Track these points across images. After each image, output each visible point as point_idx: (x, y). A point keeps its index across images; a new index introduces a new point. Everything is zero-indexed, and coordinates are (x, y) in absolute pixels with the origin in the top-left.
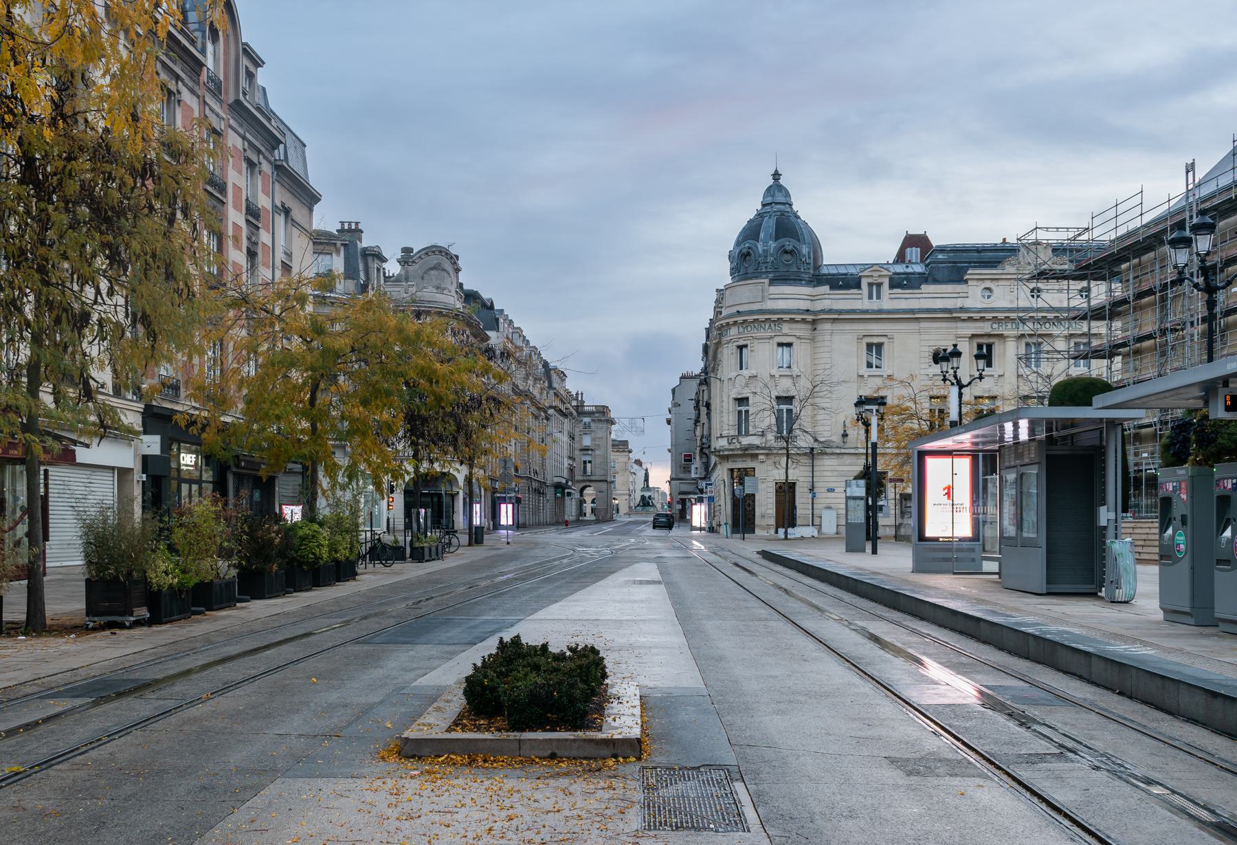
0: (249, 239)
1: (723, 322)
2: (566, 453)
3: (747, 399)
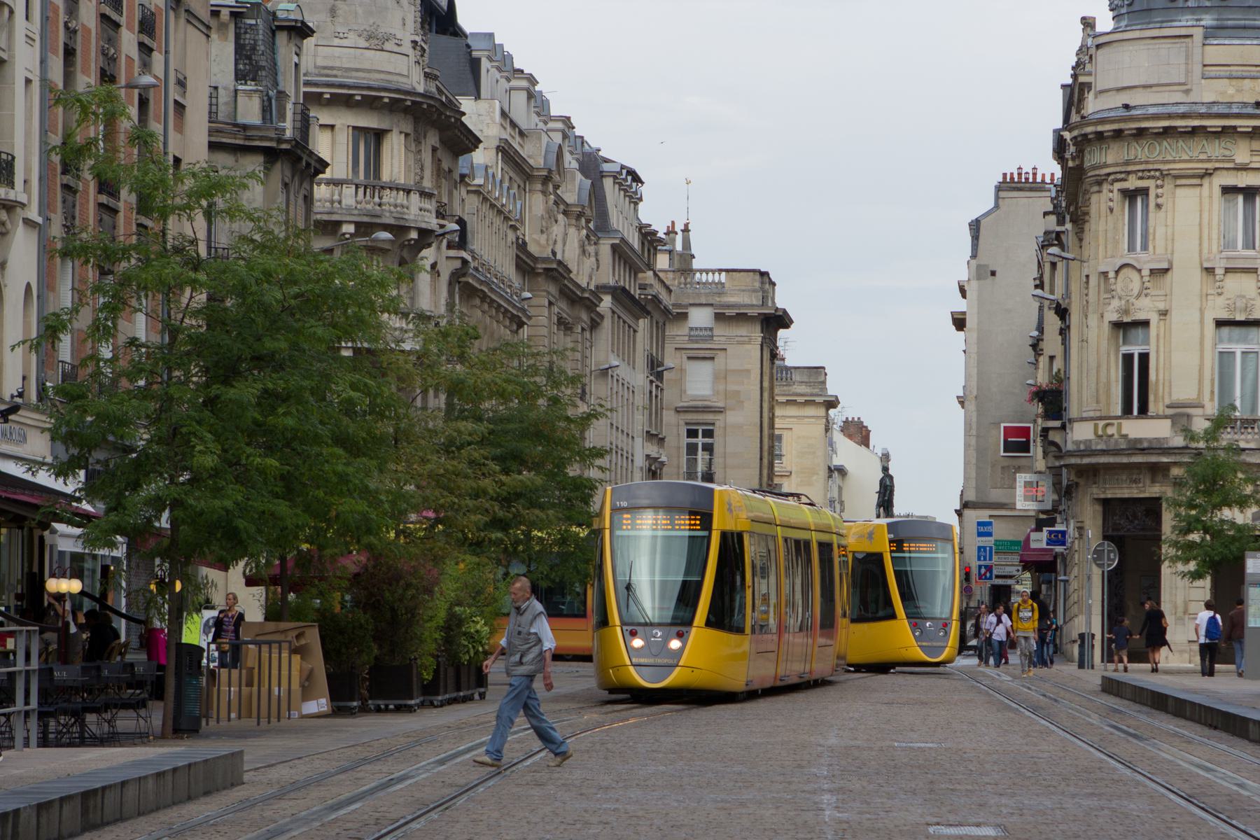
0: (67, 27)
1: (1089, 129)
2: (640, 422)
3: (1145, 324)
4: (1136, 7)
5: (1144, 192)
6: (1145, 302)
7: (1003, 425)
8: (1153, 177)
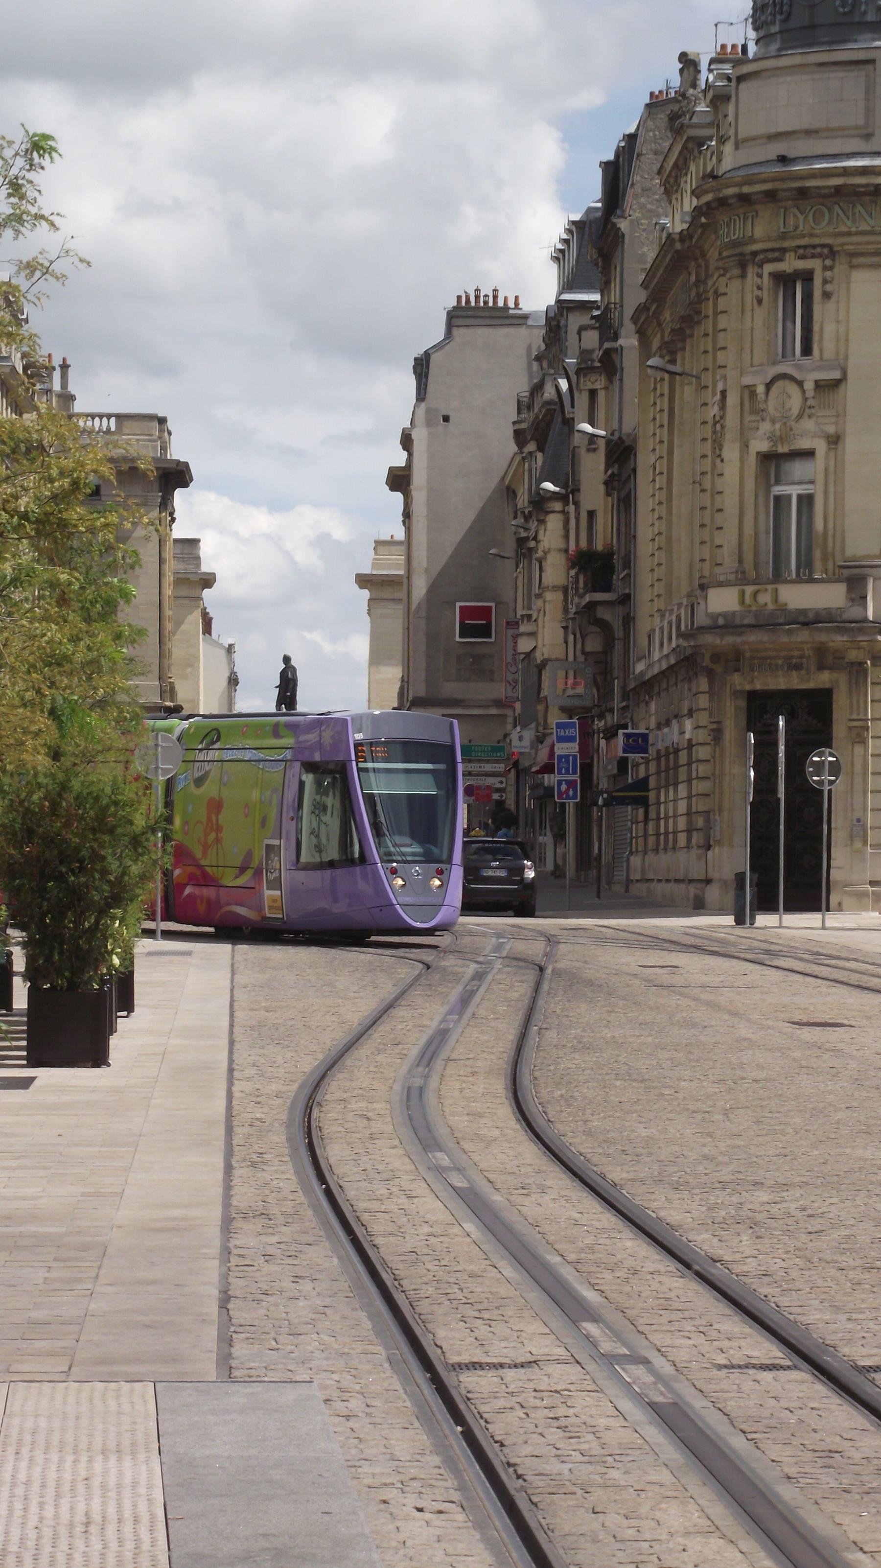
3: (809, 454)
4: (793, 23)
5: (807, 277)
6: (809, 425)
7: (458, 604)
8: (820, 256)
